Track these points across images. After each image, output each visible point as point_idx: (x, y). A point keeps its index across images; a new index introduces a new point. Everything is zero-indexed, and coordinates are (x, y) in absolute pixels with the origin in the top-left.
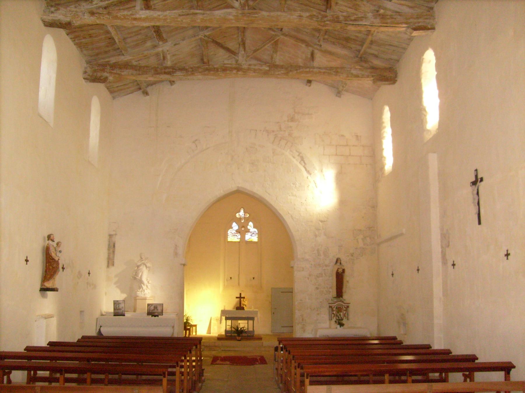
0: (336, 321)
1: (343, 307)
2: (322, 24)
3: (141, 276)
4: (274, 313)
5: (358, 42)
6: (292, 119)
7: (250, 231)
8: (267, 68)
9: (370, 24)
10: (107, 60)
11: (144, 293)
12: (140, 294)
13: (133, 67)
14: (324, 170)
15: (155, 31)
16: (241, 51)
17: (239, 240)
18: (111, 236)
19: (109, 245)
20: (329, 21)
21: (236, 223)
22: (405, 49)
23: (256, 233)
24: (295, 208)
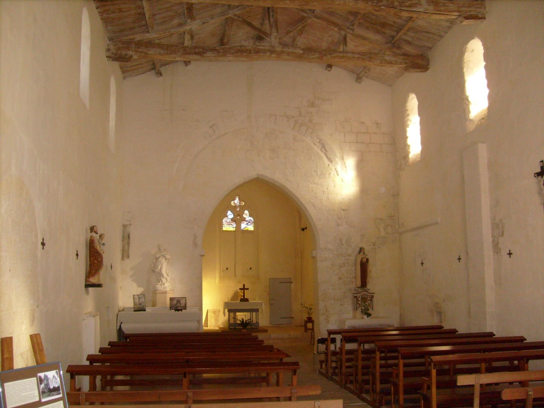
0: (362, 312)
1: (368, 297)
2: (377, 9)
3: (161, 268)
4: (272, 304)
5: (394, 28)
6: (312, 105)
7: (246, 219)
8: (301, 52)
9: (424, 10)
10: (131, 37)
11: (164, 286)
12: (159, 287)
13: (160, 46)
14: (345, 157)
15: (187, 9)
16: (274, 32)
17: (234, 229)
18: (125, 226)
19: (123, 236)
20: (385, 6)
21: (231, 212)
22: (441, 36)
23: (253, 222)
24: (317, 196)
